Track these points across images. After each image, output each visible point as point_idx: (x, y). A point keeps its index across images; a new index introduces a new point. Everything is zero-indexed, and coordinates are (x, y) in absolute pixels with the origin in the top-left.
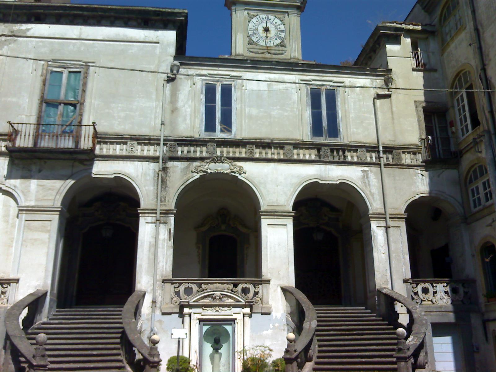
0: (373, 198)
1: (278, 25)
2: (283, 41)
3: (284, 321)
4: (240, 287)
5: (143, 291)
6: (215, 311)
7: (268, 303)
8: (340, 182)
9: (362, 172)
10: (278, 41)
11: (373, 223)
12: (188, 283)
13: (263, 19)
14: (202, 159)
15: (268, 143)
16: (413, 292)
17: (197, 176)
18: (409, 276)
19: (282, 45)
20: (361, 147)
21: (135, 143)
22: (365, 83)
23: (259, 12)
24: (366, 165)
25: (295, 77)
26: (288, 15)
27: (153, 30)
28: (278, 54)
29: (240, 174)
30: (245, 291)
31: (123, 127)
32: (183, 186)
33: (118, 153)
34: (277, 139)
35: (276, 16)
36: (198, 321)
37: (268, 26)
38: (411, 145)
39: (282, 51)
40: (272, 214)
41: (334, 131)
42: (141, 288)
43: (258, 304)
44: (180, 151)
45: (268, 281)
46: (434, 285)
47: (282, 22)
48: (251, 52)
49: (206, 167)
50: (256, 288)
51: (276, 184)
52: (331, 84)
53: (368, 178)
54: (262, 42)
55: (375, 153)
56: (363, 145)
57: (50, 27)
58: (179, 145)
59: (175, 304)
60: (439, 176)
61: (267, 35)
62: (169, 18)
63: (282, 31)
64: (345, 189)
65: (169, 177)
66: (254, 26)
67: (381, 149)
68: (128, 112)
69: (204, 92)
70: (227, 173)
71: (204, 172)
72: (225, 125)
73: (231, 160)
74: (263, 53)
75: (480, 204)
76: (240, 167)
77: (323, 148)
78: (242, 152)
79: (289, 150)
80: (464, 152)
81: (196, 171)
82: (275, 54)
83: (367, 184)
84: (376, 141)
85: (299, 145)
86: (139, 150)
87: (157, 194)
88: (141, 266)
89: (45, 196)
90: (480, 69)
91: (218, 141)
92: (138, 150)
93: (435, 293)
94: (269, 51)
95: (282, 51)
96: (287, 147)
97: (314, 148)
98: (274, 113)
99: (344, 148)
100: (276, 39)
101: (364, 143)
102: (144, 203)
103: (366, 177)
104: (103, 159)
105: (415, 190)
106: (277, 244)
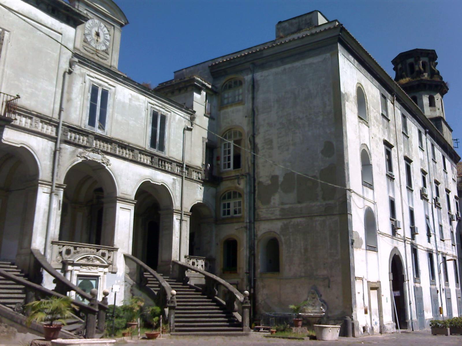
0: (176, 199)
2: (107, 49)
3: (123, 279)
4: (101, 251)
6: (88, 269)
8: (21, 147)
10: (104, 48)
12: (104, 249)
13: (96, 23)
15: (126, 145)
17: (80, 160)
18: (188, 254)
19: (106, 52)
20: (174, 162)
21: (39, 120)
23: (95, 16)
25: (146, 99)
26: (114, 29)
27: (59, 20)
28: (103, 59)
29: (107, 165)
30: (103, 255)
31: (29, 102)
33: (23, 125)
34: (132, 144)
35: (106, 26)
39: (106, 57)
40: (124, 200)
41: (162, 148)
44: (71, 136)
45: (117, 249)
48: (85, 49)
49: (87, 154)
52: (106, 85)
53: (175, 184)
55: (179, 167)
56: (176, 160)
58: (71, 131)
62: (75, 17)
64: (163, 189)
65: (61, 156)
67: (185, 166)
68: (33, 90)
69: (90, 91)
72: (101, 123)
74: (93, 54)
76: (108, 160)
77: (155, 157)
78: (108, 147)
79: (137, 154)
82: (101, 58)
84: (181, 159)
85: (143, 152)
88: (37, 228)
90: (250, 135)
91: (96, 135)
93: (197, 265)
94: (98, 54)
95: (106, 57)
96: (136, 152)
97: (149, 156)
98: (131, 122)
99: (164, 160)
100: (103, 45)
101: (177, 160)
104: (12, 128)
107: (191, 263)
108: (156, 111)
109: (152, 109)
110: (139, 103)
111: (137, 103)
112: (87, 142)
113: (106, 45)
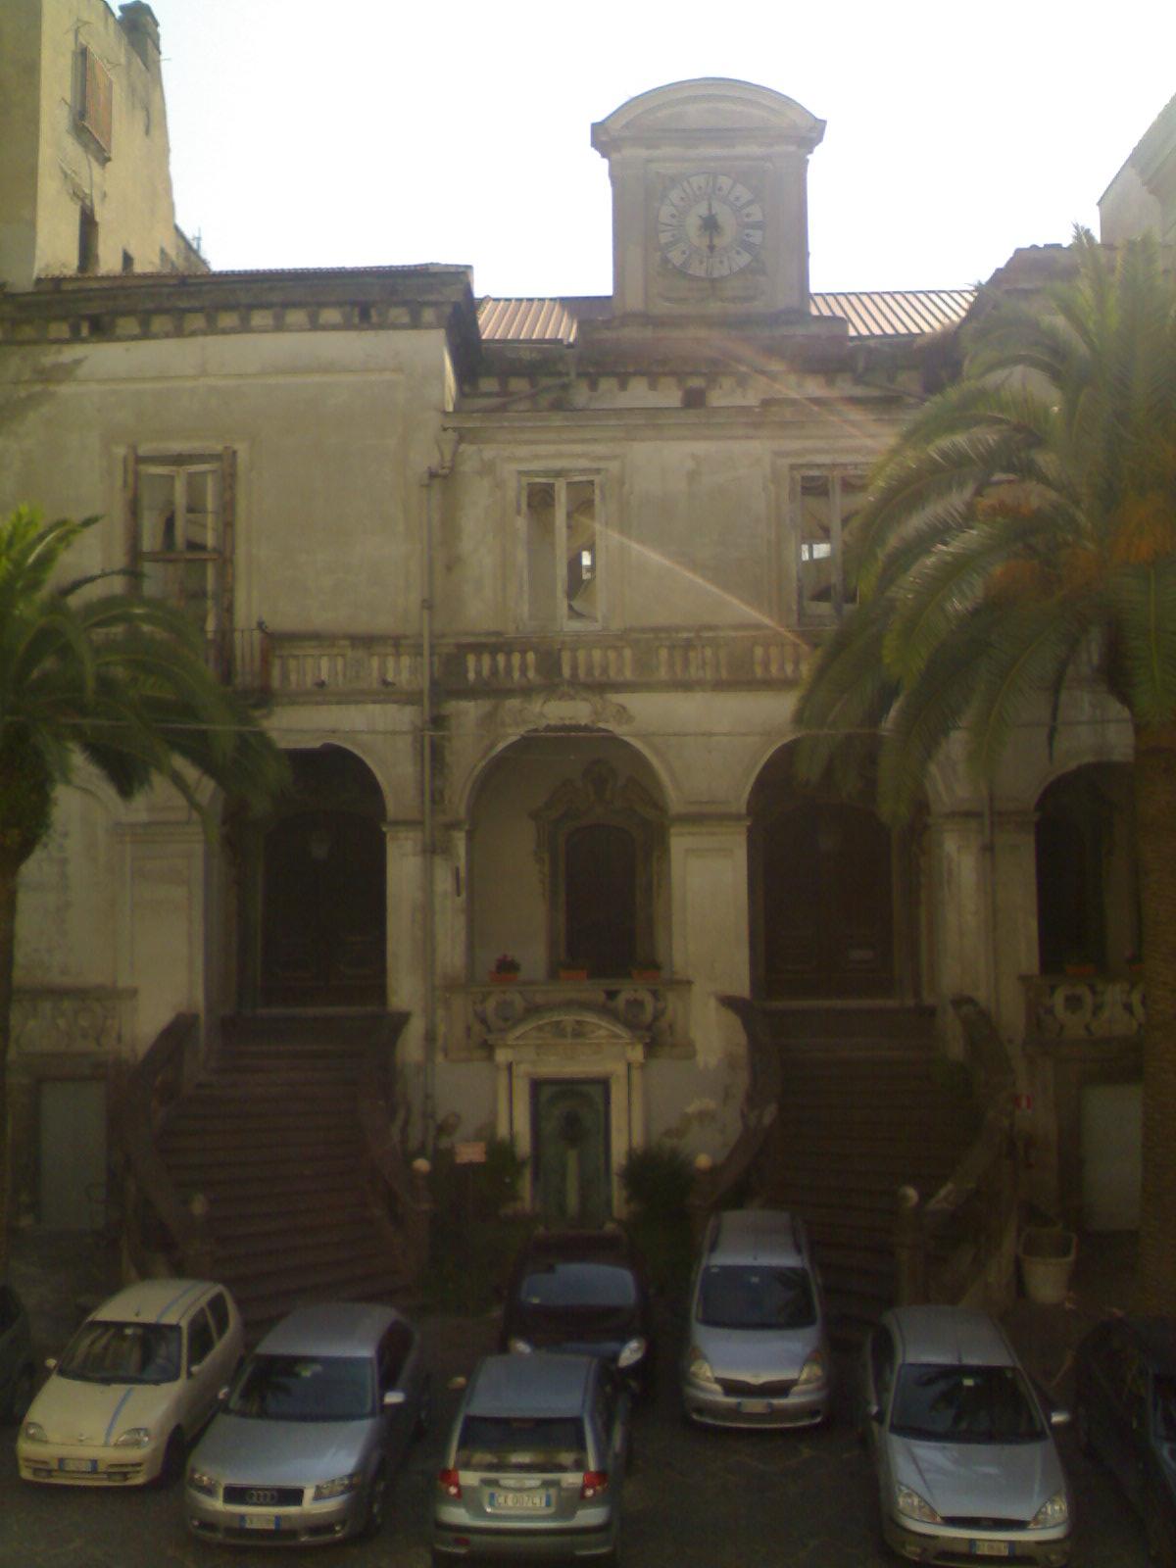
21: (346, 643)
32: (484, 763)
40: (696, 819)
57: (127, 350)
61: (711, 241)
87: (422, 783)
100: (738, 253)
108: (815, 473)
109: (795, 472)
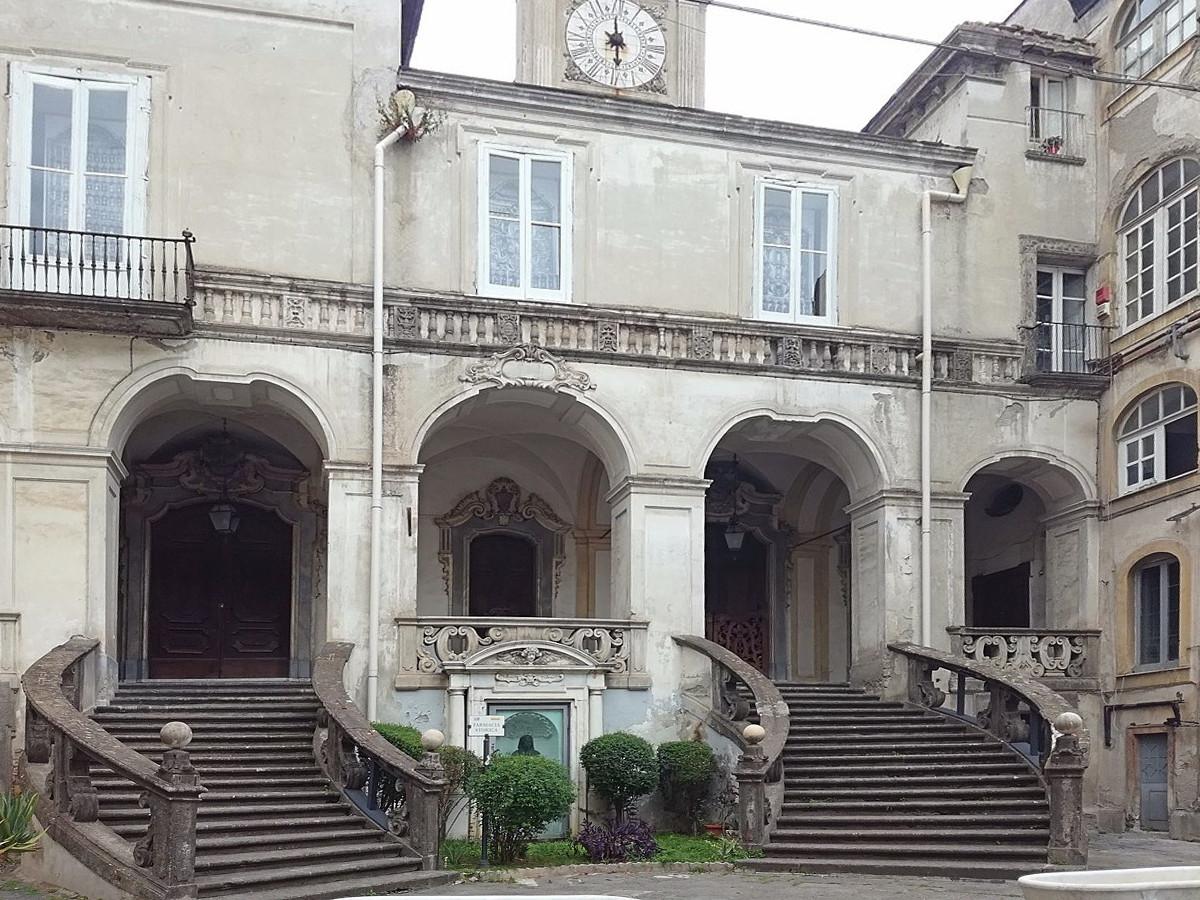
1: (647, 32)
2: (658, 78)
4: (580, 635)
5: (347, 644)
7: (642, 669)
9: (876, 399)
10: (646, 77)
11: (891, 510)
13: (607, 9)
14: (486, 351)
16: (964, 652)
17: (473, 391)
18: (961, 621)
22: (905, 183)
24: (888, 383)
33: (256, 321)
36: (485, 704)
37: (619, 32)
38: (998, 341)
42: (342, 637)
43: (621, 670)
46: (1012, 639)
47: (660, 22)
50: (614, 638)
51: (665, 423)
53: (886, 411)
54: (604, 74)
59: (425, 669)
60: (1052, 415)
63: (657, 49)
66: (581, 28)
68: (275, 218)
70: (547, 387)
71: (491, 380)
73: (559, 356)
75: (1148, 475)
80: (1126, 360)
81: (470, 379)
83: (885, 426)
86: (316, 319)
89: (61, 421)
92: (312, 318)
100: (641, 70)
101: (888, 332)
102: (337, 448)
103: (883, 410)
105: (994, 441)
106: (664, 552)
107: (979, 647)
110: (698, 178)
111: (691, 179)
112: (495, 335)
113: (652, 68)
